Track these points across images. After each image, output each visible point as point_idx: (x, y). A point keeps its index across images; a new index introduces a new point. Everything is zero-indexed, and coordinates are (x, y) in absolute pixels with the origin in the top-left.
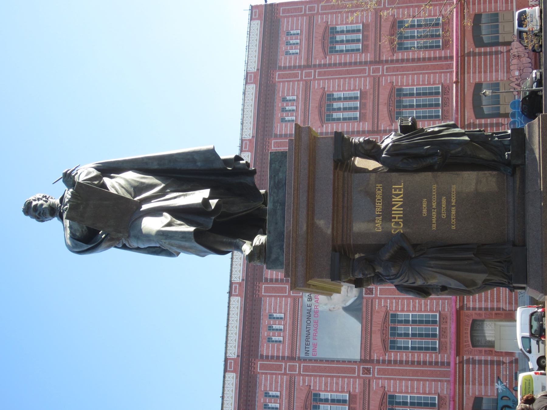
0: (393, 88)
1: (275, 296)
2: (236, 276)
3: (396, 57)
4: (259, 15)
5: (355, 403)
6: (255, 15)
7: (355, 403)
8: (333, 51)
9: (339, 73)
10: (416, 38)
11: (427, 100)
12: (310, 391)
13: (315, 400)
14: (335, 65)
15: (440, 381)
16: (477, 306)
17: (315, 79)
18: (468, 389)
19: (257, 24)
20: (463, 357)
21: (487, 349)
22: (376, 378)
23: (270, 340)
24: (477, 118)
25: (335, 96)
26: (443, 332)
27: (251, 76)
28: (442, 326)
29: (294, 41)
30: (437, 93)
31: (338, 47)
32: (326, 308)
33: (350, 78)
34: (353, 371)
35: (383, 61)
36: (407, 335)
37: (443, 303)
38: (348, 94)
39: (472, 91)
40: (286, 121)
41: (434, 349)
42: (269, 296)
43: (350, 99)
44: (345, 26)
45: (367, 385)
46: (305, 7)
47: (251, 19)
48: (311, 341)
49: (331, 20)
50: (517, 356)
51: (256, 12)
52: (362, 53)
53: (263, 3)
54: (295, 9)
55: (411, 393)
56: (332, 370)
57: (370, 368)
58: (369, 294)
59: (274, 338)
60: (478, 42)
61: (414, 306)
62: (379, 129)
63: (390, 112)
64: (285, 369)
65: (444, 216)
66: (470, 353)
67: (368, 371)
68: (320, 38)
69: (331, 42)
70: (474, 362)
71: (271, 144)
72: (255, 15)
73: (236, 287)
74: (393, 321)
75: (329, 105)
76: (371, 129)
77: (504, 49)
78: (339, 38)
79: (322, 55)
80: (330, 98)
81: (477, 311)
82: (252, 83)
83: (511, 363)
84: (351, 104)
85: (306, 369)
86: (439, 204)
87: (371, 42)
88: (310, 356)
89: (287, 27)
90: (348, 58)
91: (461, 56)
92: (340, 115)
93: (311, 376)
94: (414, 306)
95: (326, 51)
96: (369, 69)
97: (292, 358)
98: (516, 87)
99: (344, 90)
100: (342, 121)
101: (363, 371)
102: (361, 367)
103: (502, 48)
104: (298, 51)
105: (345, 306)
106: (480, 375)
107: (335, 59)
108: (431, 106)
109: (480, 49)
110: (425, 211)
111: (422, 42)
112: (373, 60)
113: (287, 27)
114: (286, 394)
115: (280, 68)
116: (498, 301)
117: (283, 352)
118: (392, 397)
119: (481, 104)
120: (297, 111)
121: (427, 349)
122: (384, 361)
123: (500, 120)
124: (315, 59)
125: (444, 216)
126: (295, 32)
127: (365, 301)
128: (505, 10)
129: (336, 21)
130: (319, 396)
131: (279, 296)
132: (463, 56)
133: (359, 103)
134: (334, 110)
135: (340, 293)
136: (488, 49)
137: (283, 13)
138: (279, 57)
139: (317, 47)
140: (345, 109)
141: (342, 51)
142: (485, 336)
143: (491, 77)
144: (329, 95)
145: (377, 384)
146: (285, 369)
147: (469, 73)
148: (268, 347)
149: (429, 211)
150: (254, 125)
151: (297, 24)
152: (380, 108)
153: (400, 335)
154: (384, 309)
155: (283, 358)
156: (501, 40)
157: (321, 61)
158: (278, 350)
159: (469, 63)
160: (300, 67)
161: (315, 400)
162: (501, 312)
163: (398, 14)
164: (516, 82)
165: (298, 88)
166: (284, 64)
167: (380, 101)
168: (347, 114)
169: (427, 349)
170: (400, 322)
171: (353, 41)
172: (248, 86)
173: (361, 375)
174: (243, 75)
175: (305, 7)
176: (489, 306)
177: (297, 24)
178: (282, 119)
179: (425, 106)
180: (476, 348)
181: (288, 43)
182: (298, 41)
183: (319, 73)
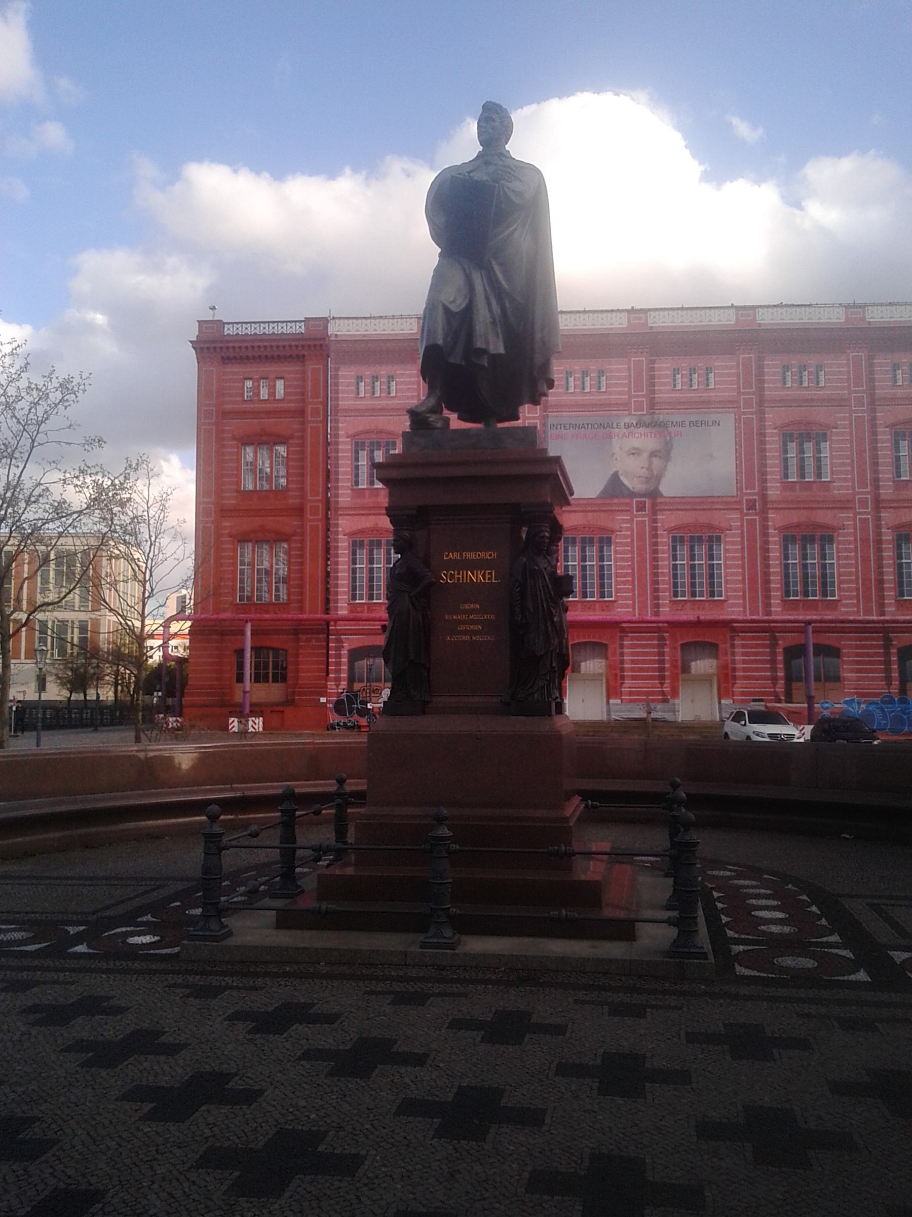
0: (833, 529)
3: (662, 535)
16: (625, 650)
21: (679, 664)
23: (359, 379)
25: (806, 445)
26: (813, 606)
28: (597, 605)
31: (792, 446)
32: (616, 449)
35: (880, 512)
36: (584, 559)
37: (627, 606)
42: (629, 369)
50: (671, 701)
52: (894, 481)
58: (637, 507)
59: (571, 379)
61: (623, 568)
62: (340, 518)
64: (638, 396)
70: (661, 646)
73: (639, 318)
74: (601, 540)
76: (882, 497)
81: (618, 651)
92: (792, 454)
94: (623, 568)
102: (869, 496)
104: (695, 387)
105: (620, 473)
112: (882, 497)
116: (633, 678)
118: (609, 541)
121: (675, 585)
123: (896, 683)
127: (628, 501)
136: (345, 667)
146: (638, 396)
147: (856, 639)
153: (692, 549)
154: (617, 527)
158: (665, 384)
162: (619, 682)
169: (675, 585)
170: (601, 550)
172: (732, 312)
173: (857, 497)
176: (737, 666)
178: (361, 377)
180: (679, 648)
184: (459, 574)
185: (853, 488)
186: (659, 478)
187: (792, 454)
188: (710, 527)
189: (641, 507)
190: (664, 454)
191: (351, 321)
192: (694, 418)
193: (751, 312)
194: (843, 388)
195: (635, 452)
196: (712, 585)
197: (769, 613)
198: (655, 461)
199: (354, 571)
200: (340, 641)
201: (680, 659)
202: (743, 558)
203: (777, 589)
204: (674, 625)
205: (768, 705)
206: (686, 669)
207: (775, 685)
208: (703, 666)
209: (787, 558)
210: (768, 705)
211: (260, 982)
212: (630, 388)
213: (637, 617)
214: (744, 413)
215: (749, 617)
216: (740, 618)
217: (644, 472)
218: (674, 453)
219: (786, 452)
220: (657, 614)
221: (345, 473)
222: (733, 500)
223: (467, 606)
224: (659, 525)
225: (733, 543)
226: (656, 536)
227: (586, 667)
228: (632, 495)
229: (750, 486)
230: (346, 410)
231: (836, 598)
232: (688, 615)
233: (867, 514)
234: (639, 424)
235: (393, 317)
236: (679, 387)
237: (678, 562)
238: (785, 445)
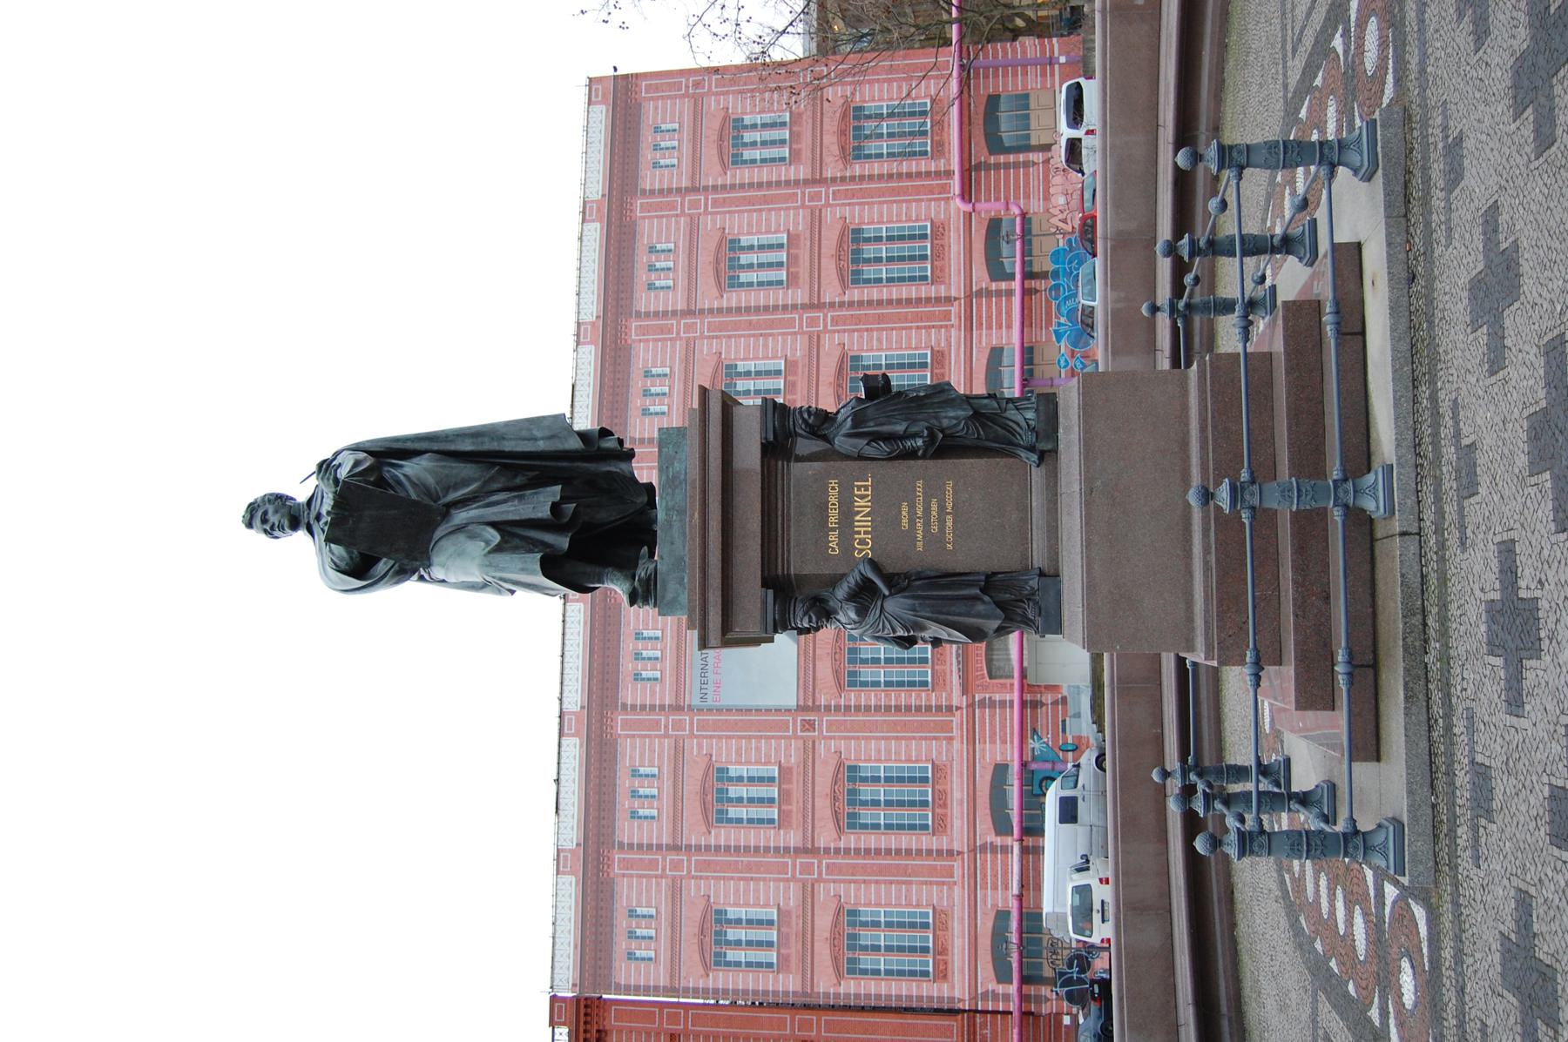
0: (844, 229)
4: (604, 95)
5: (796, 374)
7: (798, 247)
8: (738, 161)
9: (750, 201)
11: (905, 248)
12: (708, 905)
13: (718, 921)
14: (742, 186)
15: (936, 738)
17: (706, 212)
18: (984, 750)
19: (601, 112)
22: (825, 738)
24: (992, 280)
27: (566, 858)
30: (924, 365)
31: (733, 812)
33: (770, 210)
34: (784, 726)
38: (766, 239)
39: (988, 778)
41: (925, 684)
43: (771, 247)
45: (809, 750)
48: (711, 677)
49: (737, 105)
50: (1065, 692)
53: (612, 73)
55: (887, 761)
56: (748, 726)
60: (996, 145)
63: (840, 270)
64: (666, 727)
65: (935, 528)
66: (985, 689)
69: (732, 267)
70: (992, 704)
75: (718, 933)
76: (807, 301)
78: (748, 137)
79: (719, 168)
83: (1055, 703)
84: (771, 257)
86: (927, 510)
87: (805, 144)
88: (710, 702)
89: (655, 118)
90: (765, 174)
92: (753, 277)
93: (711, 737)
96: (794, 865)
97: (677, 708)
98: (1061, 225)
99: (759, 232)
104: (675, 161)
106: (1003, 727)
107: (743, 175)
108: (912, 258)
110: (905, 521)
111: (895, 669)
113: (655, 118)
115: (644, 192)
117: (659, 836)
121: (912, 684)
124: (707, 175)
125: (935, 528)
126: (669, 126)
132: (969, 172)
134: (745, 145)
136: (1012, 158)
139: (710, 153)
140: (764, 143)
141: (753, 161)
143: (1015, 84)
144: (720, 770)
145: (828, 749)
146: (666, 727)
148: (631, 827)
149: (912, 522)
151: (673, 112)
153: (864, 803)
155: (659, 847)
156: (1034, 142)
158: (653, 693)
159: (978, 183)
160: (679, 190)
161: (720, 779)
163: (848, 748)
164: (1061, 216)
165: (678, 229)
167: (825, 127)
168: (766, 275)
169: (912, 684)
170: (864, 780)
171: (770, 265)
172: (588, 226)
174: (551, 853)
177: (673, 112)
179: (901, 259)
181: (656, 147)
182: (675, 143)
183: (715, 201)
185: (787, 880)
188: (844, 116)
194: (673, 347)
199: (889, 972)
200: (985, 995)
202: (877, 882)
203: (919, 697)
209: (877, 972)
211: (1445, 408)
212: (676, 97)
214: (689, 871)
221: (757, 836)
225: (860, 343)
230: (672, 976)
233: (824, 318)
235: (555, 907)
238: (741, 285)
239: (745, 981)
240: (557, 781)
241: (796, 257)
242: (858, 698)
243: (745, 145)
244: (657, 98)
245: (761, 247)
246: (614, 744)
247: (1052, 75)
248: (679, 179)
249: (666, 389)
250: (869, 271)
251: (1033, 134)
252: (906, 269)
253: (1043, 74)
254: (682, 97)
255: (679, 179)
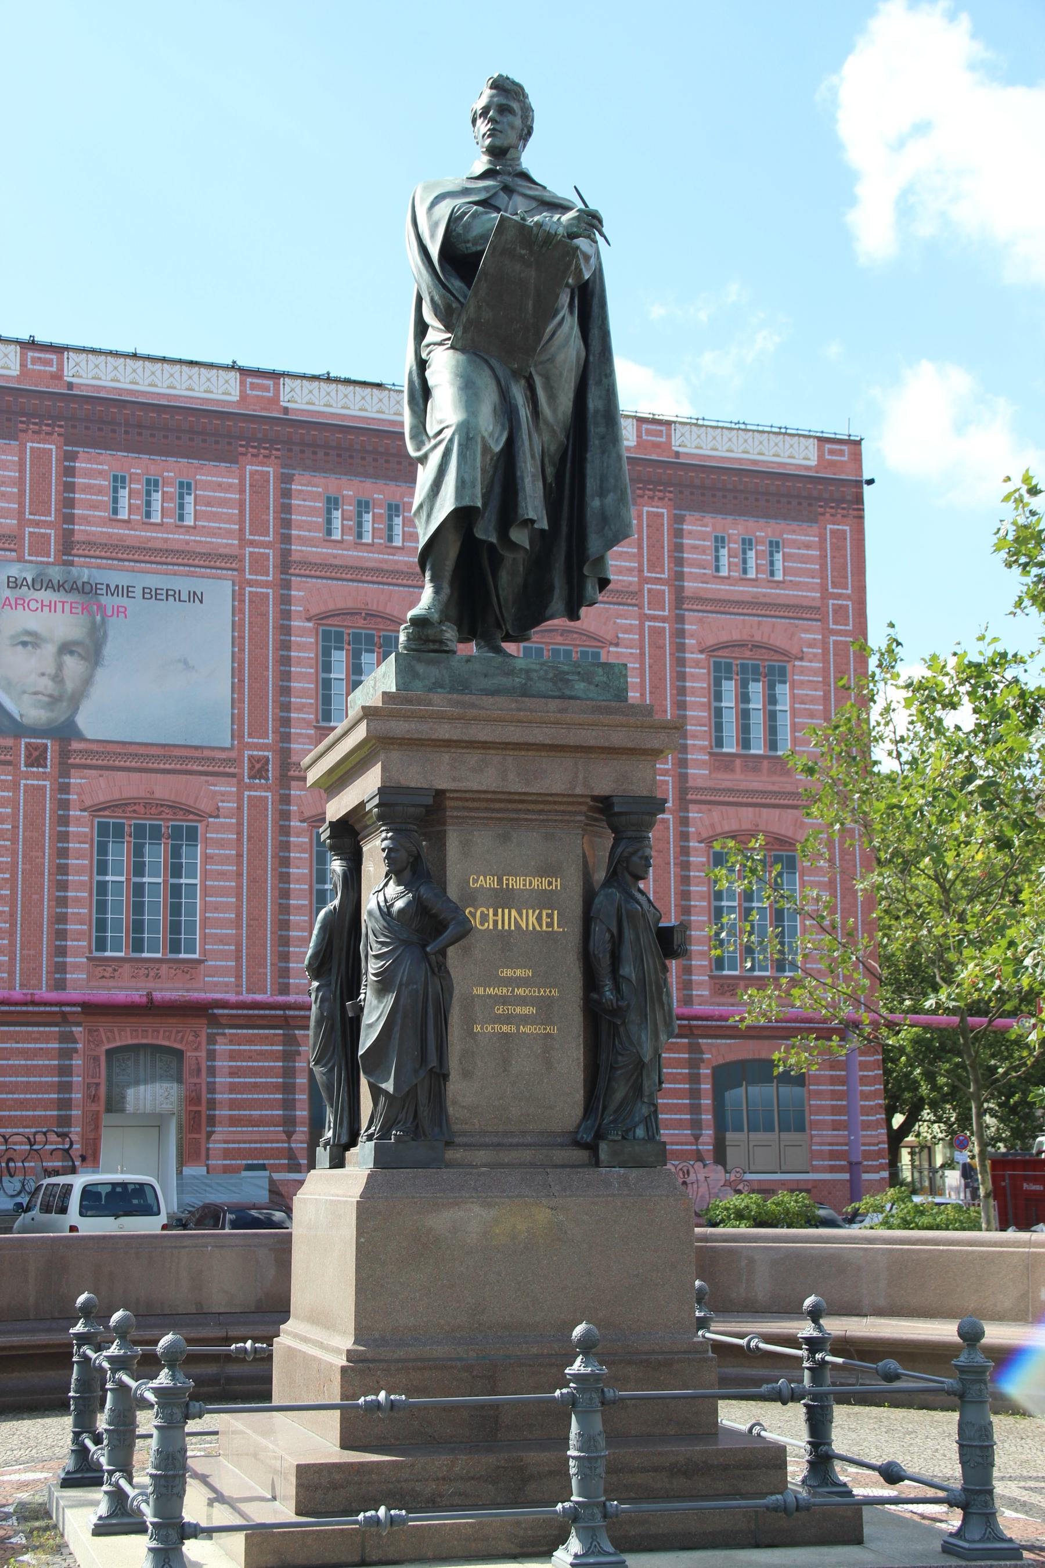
1: (21, 480)
2: (83, 364)
3: (696, 849)
4: (832, 464)
6: (832, 452)
8: (720, 672)
10: (747, 905)
11: (157, 916)
19: (804, 457)
20: (78, 1024)
21: (103, 1091)
27: (659, 434)
29: (752, 563)
31: (729, 687)
35: (687, 810)
38: (784, 721)
40: (329, 512)
41: (101, 945)
44: (787, 708)
46: (848, 597)
47: (822, 440)
49: (808, 670)
51: (841, 453)
52: (711, 754)
54: (844, 567)
57: (46, 767)
62: (293, 783)
64: (37, 524)
67: (259, 771)
68: (758, 638)
69: (744, 668)
70: (66, 1054)
71: (262, 464)
72: (832, 452)
73: (49, 363)
75: (756, 669)
77: (706, 1144)
78: (756, 689)
79: (711, 641)
80: (775, 676)
82: (639, 436)
83: (291, 1154)
85: (259, 601)
87: (738, 779)
89: (794, 544)
91: (286, 1018)
92: (729, 702)
95: (720, 653)
100: (322, 675)
101: (36, 747)
103: (710, 1140)
104: (724, 572)
107: (305, 643)
109: (710, 1080)
112: (691, 783)
113: (794, 544)
114: (396, 562)
116: (234, 1121)
119: (752, 1082)
120: (358, 544)
121: (101, 925)
122: (65, 805)
124: (701, 621)
126: (779, 565)
128: (812, 1151)
129: (802, 682)
130: (336, 648)
131: (22, 493)
133: (761, 752)
135: (384, 693)
136: (707, 1102)
137: (832, 531)
138: (709, 519)
139: (730, 628)
141: (718, 697)
142: (137, 1083)
144: (783, 672)
146: (37, 524)
150: (755, 462)
152: (743, 810)
153: (138, 851)
156: (730, 1136)
157: (692, 636)
158: (94, 506)
160: (680, 576)
162: (205, 1129)
166: (690, 532)
167: (765, 811)
168: (730, 719)
169: (101, 925)
172: (812, 444)
175: (848, 597)
180: (103, 1058)
181: (747, 543)
182: (752, 574)
184: (495, 914)
186: (76, 700)
187: (729, 702)
188: (176, 808)
189: (36, 758)
190: (91, 649)
191: (196, 369)
192: (153, 581)
193: (270, 383)
195: (30, 641)
196: (175, 928)
197: (284, 989)
198: (70, 661)
201: (103, 1080)
202: (239, 874)
204: (92, 1009)
205: (276, 1176)
206: (114, 1105)
207: (289, 1135)
208: (153, 1095)
210: (276, 1176)
212: (824, 578)
213: (18, 994)
214: (251, 583)
215: (247, 997)
216: (231, 997)
217: (45, 684)
218: (109, 650)
219: (327, 667)
220: (60, 985)
222: (224, 755)
223: (508, 973)
224: (73, 797)
225: (221, 844)
226: (64, 821)
227: (137, 1099)
228: (19, 729)
229: (258, 730)
231: (196, 956)
232: (126, 990)
234: (41, 583)
236: (123, 515)
237: (109, 878)
239: (302, 677)
240: (135, 356)
241: (756, 770)
242: (81, 838)
243: (744, 684)
244: (822, 548)
245: (772, 716)
246: (813, 519)
247: (832, 1169)
248: (696, 578)
249: (367, 539)
250: (120, 854)
251: (742, 1136)
252: (120, 915)
253: (833, 1155)
254: (823, 588)
255: (696, 578)
